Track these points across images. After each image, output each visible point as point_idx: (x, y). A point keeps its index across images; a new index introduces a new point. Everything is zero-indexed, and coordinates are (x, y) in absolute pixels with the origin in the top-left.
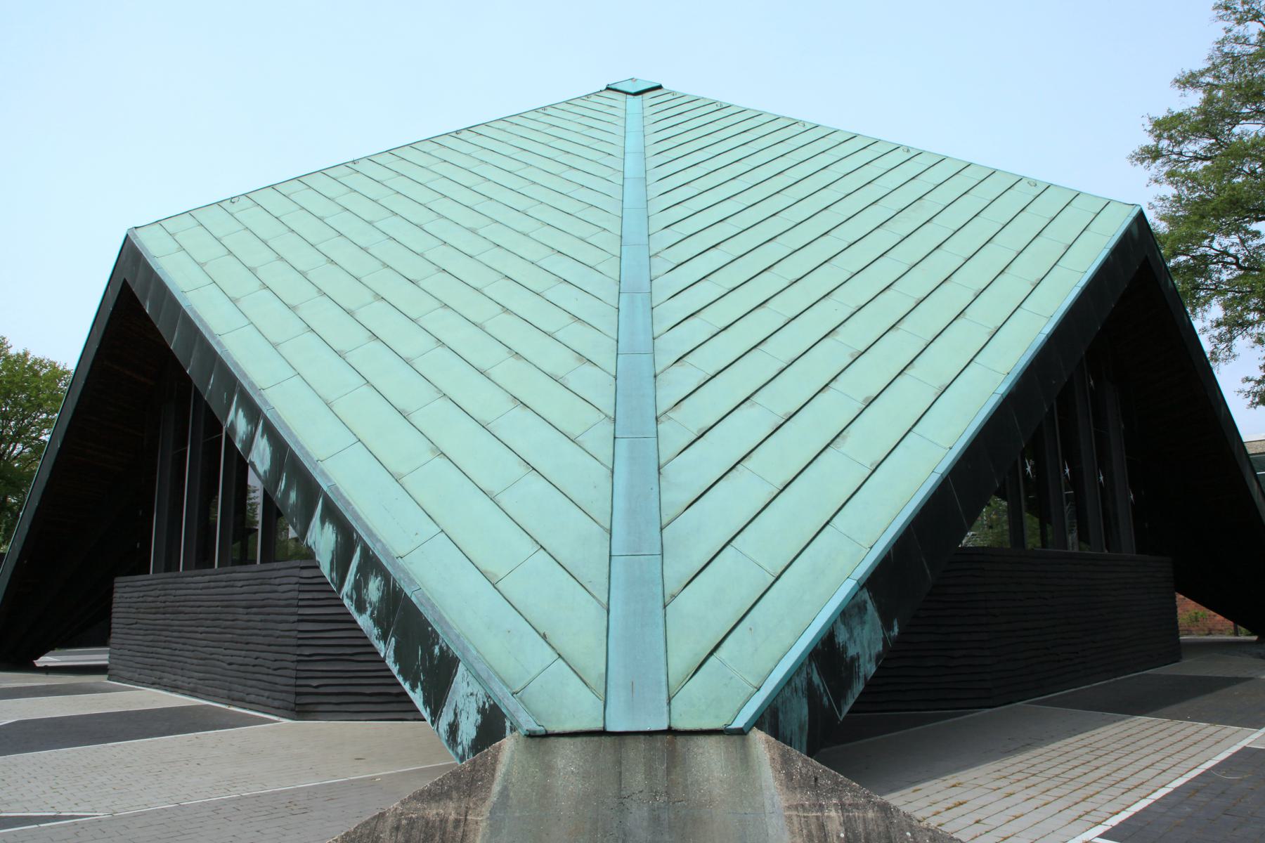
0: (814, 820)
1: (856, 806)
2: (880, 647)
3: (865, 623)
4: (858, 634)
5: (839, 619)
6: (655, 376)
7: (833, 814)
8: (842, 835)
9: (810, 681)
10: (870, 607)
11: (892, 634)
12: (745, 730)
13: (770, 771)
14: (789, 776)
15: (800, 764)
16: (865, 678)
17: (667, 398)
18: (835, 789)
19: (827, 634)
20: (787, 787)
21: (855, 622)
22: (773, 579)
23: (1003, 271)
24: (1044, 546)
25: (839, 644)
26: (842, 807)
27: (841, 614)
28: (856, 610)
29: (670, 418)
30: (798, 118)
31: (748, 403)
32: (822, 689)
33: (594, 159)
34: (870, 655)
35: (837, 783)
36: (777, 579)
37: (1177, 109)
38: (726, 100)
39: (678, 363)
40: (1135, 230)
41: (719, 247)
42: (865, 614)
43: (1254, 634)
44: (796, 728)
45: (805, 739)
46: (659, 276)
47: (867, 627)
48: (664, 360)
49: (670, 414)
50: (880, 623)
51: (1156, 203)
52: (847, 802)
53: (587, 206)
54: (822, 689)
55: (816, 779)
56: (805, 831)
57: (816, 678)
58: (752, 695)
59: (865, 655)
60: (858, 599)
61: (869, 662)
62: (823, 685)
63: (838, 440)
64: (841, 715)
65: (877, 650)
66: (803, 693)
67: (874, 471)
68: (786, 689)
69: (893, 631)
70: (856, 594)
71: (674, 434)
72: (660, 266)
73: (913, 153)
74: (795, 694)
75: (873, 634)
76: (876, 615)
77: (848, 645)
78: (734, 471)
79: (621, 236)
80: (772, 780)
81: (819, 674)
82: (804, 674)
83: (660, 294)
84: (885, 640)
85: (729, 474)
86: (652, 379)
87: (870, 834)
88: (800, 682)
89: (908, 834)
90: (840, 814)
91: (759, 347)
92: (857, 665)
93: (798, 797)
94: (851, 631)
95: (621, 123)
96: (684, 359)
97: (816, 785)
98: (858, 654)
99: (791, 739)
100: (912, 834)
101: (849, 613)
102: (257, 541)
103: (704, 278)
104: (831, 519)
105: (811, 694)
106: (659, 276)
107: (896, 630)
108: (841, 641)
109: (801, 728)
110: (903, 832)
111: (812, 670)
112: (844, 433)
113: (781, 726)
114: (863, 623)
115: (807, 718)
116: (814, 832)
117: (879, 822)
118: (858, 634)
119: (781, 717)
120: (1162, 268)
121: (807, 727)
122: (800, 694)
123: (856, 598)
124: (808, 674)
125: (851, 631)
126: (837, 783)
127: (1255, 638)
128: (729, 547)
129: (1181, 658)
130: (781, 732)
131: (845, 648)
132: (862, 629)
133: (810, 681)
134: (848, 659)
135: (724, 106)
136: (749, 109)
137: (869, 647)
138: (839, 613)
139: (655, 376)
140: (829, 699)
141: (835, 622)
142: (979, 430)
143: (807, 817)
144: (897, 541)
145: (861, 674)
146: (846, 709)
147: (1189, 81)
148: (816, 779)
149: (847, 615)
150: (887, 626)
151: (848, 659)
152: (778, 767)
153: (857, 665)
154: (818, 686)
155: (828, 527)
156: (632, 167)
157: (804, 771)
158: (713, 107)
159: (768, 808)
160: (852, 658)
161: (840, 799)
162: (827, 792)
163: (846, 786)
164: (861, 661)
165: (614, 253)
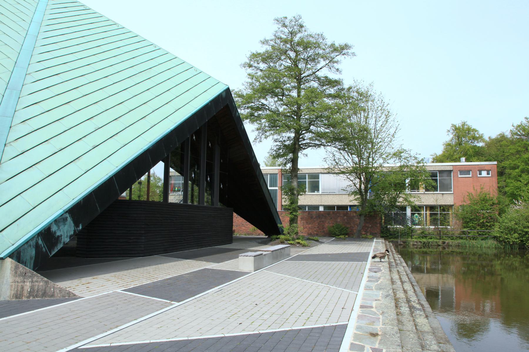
0: (21, 286)
1: (37, 281)
2: (72, 233)
3: (66, 224)
4: (62, 228)
5: (54, 222)
6: (11, 127)
7: (28, 284)
8: (29, 290)
9: (37, 243)
10: (69, 219)
11: (78, 229)
12: (4, 258)
13: (9, 271)
14: (16, 273)
15: (21, 269)
16: (64, 243)
17: (13, 136)
18: (32, 277)
19: (47, 227)
20: (14, 276)
21: (61, 224)
22: (32, 208)
23: (167, 103)
24: (199, 204)
25: (53, 231)
26: (32, 282)
27: (54, 221)
28: (62, 220)
29: (11, 145)
30: (117, 22)
31: (46, 142)
32: (43, 246)
33: (15, 21)
34: (67, 235)
35: (33, 275)
36: (34, 208)
37: (259, 52)
38: (89, 5)
39: (23, 123)
40: (224, 95)
41: (59, 75)
42: (66, 222)
43: (266, 235)
44: (28, 258)
45: (32, 262)
46: (27, 84)
47: (66, 227)
48: (17, 121)
49: (12, 144)
50: (73, 225)
51: (244, 84)
52: (34, 280)
53: (4, 44)
54: (43, 246)
55: (26, 273)
56: (16, 289)
57: (40, 242)
58: (9, 247)
59: (64, 235)
60: (64, 216)
61: (66, 238)
62: (44, 245)
63: (77, 160)
64: (51, 255)
65: (70, 234)
66: (33, 247)
67: (86, 173)
68: (25, 245)
69: (79, 228)
70: (63, 215)
71: (10, 152)
72: (29, 79)
73: (157, 48)
74: (29, 247)
75: (69, 228)
76: (72, 222)
77: (57, 231)
78: (31, 168)
79: (16, 62)
80: (9, 274)
81: (42, 240)
82: (35, 241)
83: (25, 92)
84: (75, 231)
85: (29, 169)
86: (9, 128)
87: (39, 290)
88: (33, 243)
89: (52, 289)
90: (30, 284)
91: (59, 121)
92: (60, 238)
93: (17, 279)
94: (59, 227)
95: (35, 5)
96: (26, 122)
97: (25, 275)
98: (61, 235)
99: (26, 262)
100: (53, 289)
101: (59, 221)
102: (190, 162)
103: (47, 88)
104: (63, 188)
105: (37, 247)
106: (27, 84)
107: (81, 227)
108: (53, 230)
109: (31, 258)
110: (51, 289)
111: (39, 239)
112: (80, 158)
113: (21, 257)
114: (65, 224)
115: (34, 255)
116: (19, 289)
117: (43, 286)
118: (62, 228)
119: (22, 254)
120: (234, 108)
121: (34, 258)
122: (32, 247)
123: (62, 216)
124: (36, 240)
125: (59, 227)
126: (33, 275)
127: (267, 237)
128: (19, 196)
129: (232, 242)
130: (21, 259)
131: (55, 233)
132: (64, 227)
133: (37, 243)
134: (56, 236)
135: (87, 9)
136: (98, 13)
137: (67, 232)
138: (54, 220)
139: (11, 127)
140: (46, 249)
141: (52, 223)
142: (130, 162)
143: (18, 285)
144: (85, 197)
145: (62, 242)
146: (53, 253)
147: (265, 42)
148: (26, 273)
149: (57, 222)
150: (76, 225)
151: (56, 236)
152: (13, 270)
153: (60, 238)
154: (41, 245)
155: (61, 191)
156: (33, 30)
157: (22, 271)
158: (82, 8)
159: (5, 282)
160: (58, 236)
161: (32, 279)
162: (28, 277)
163: (36, 275)
164: (62, 237)
165: (10, 70)
